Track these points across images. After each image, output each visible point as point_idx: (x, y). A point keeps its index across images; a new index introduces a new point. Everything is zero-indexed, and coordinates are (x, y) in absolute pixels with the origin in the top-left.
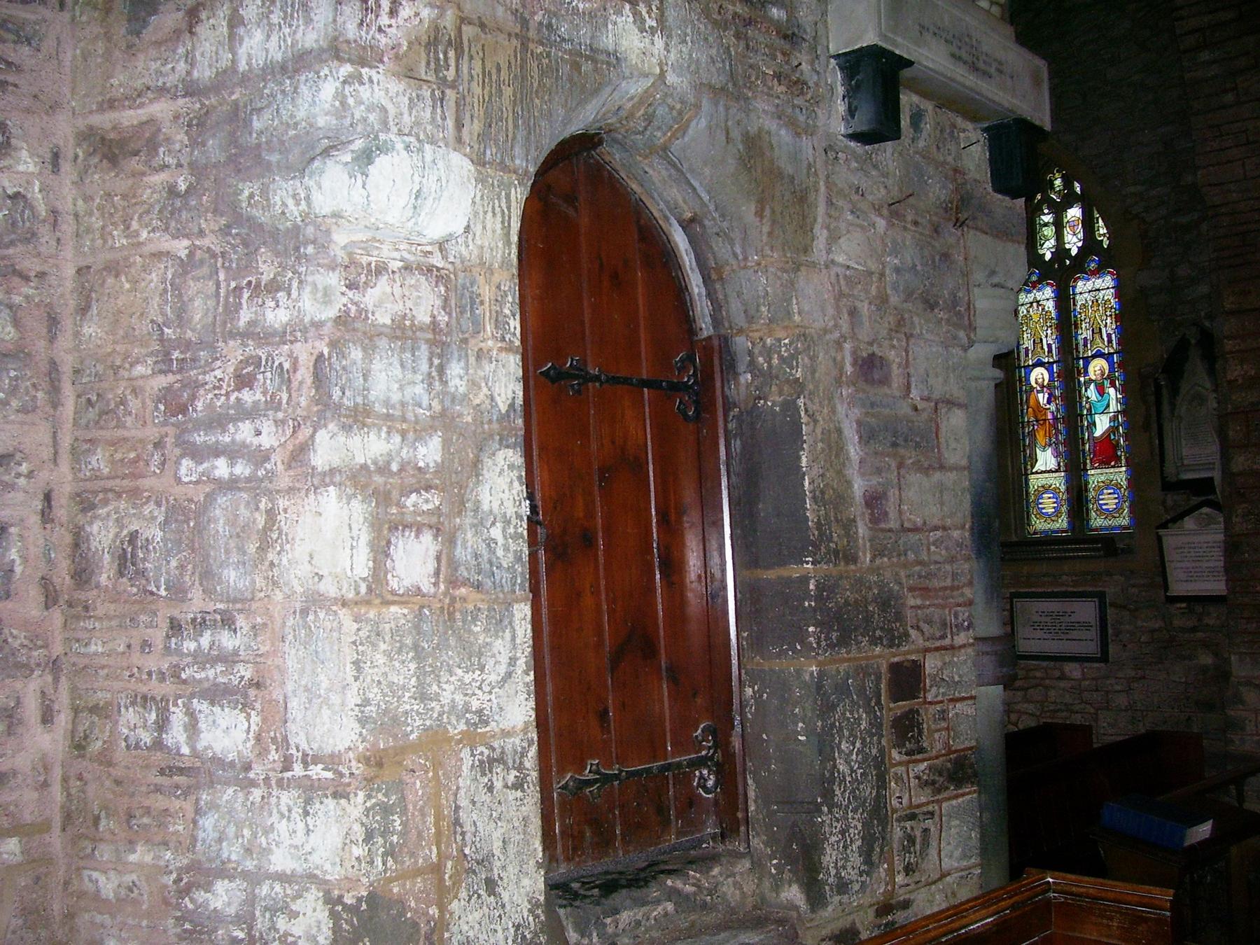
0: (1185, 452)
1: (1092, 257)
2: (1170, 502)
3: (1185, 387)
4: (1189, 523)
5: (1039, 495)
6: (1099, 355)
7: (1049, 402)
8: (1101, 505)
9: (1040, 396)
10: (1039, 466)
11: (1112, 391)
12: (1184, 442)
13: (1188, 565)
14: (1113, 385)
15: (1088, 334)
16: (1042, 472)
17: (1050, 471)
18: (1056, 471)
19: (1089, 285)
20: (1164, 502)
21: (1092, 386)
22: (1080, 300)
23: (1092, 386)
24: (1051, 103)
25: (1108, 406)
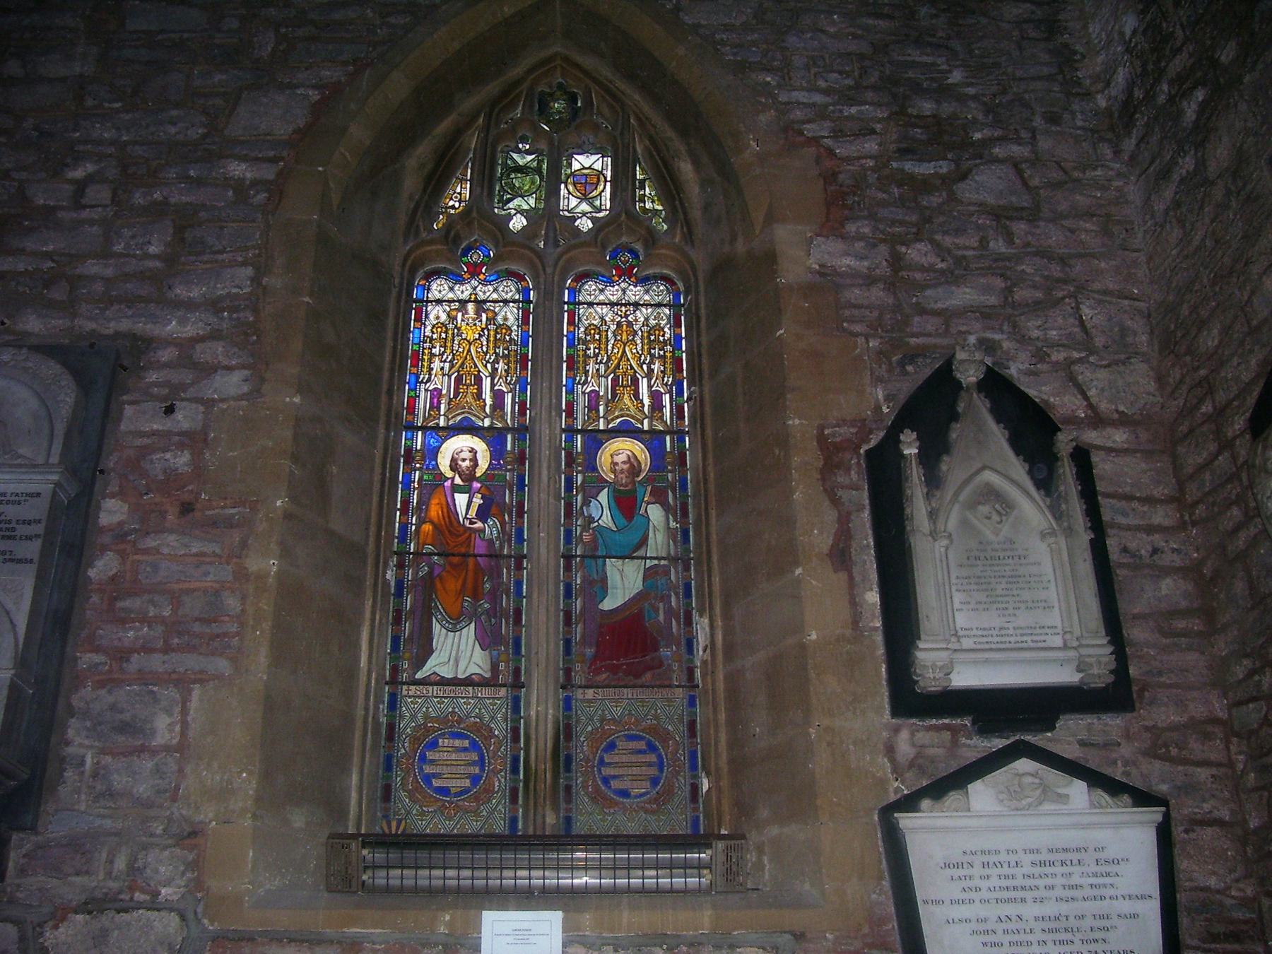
0: (961, 620)
1: (619, 247)
2: (905, 748)
3: (953, 469)
4: (981, 793)
5: (426, 740)
6: (626, 430)
7: (483, 514)
8: (428, 779)
9: (461, 500)
10: (437, 664)
11: (655, 513)
12: (958, 598)
13: (982, 911)
14: (659, 497)
15: (603, 387)
16: (443, 682)
17: (468, 682)
18: (484, 683)
19: (613, 293)
20: (890, 750)
21: (603, 497)
22: (589, 317)
23: (603, 497)
24: (6, 867)
25: (643, 542)
